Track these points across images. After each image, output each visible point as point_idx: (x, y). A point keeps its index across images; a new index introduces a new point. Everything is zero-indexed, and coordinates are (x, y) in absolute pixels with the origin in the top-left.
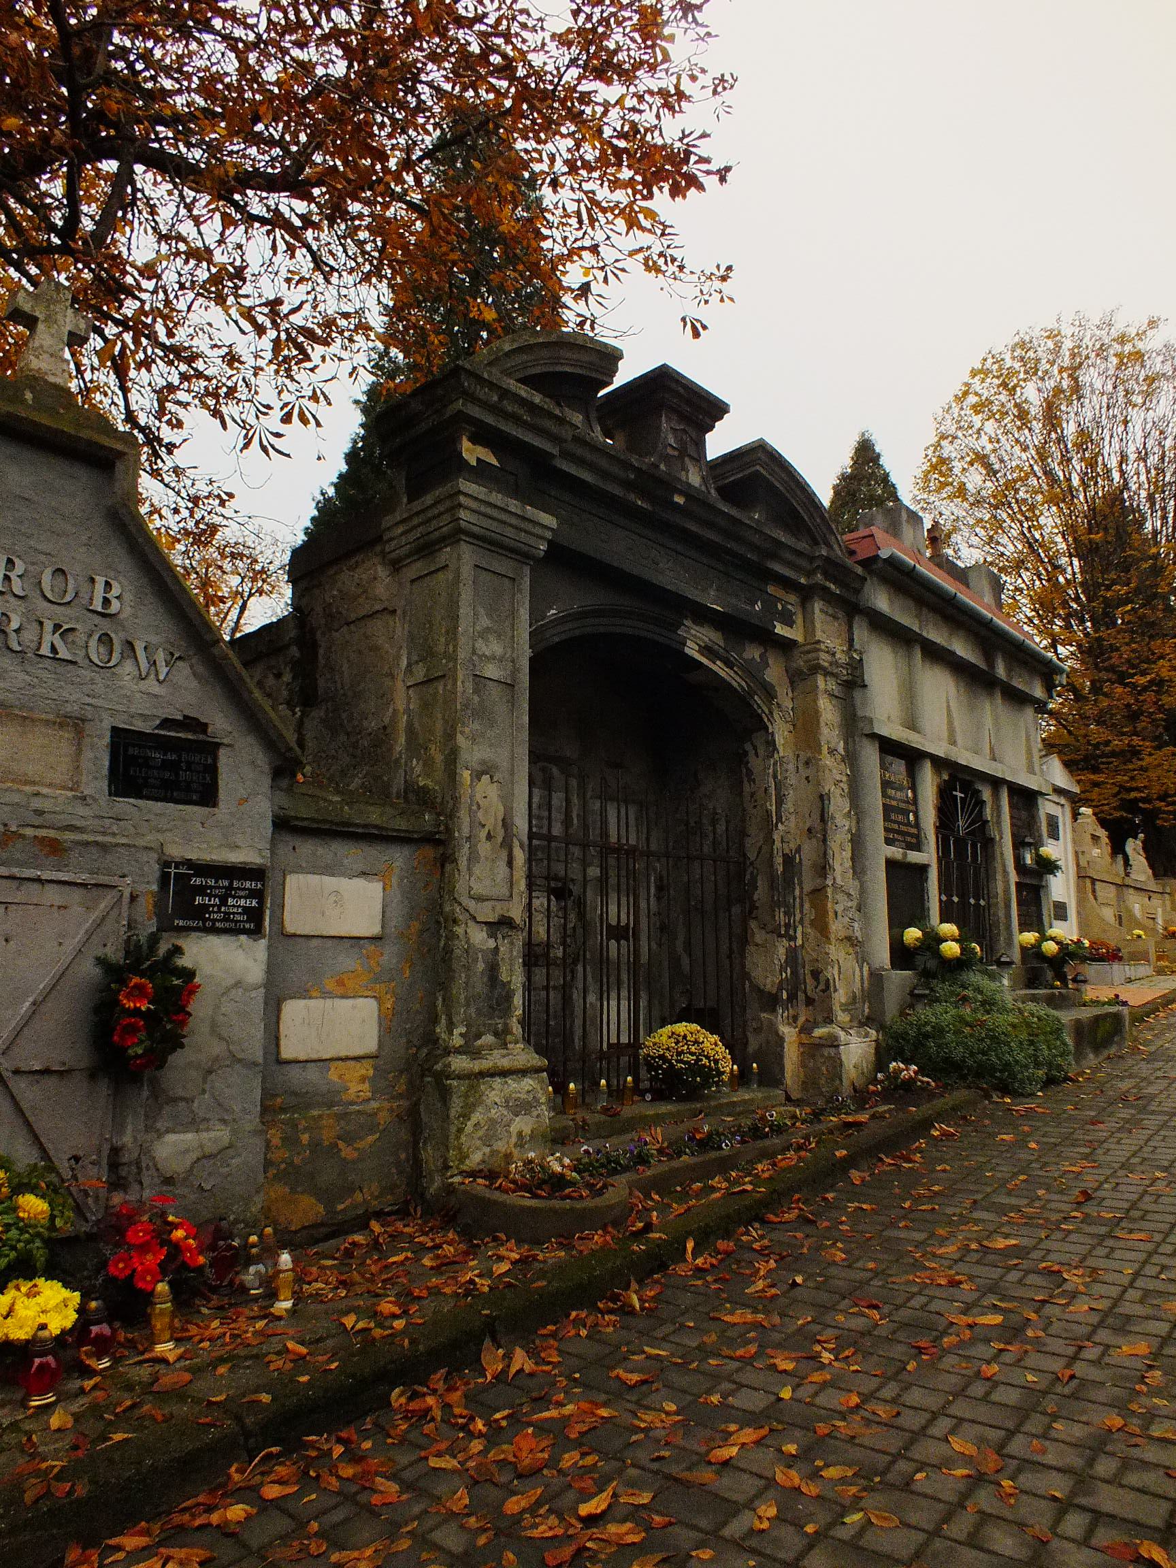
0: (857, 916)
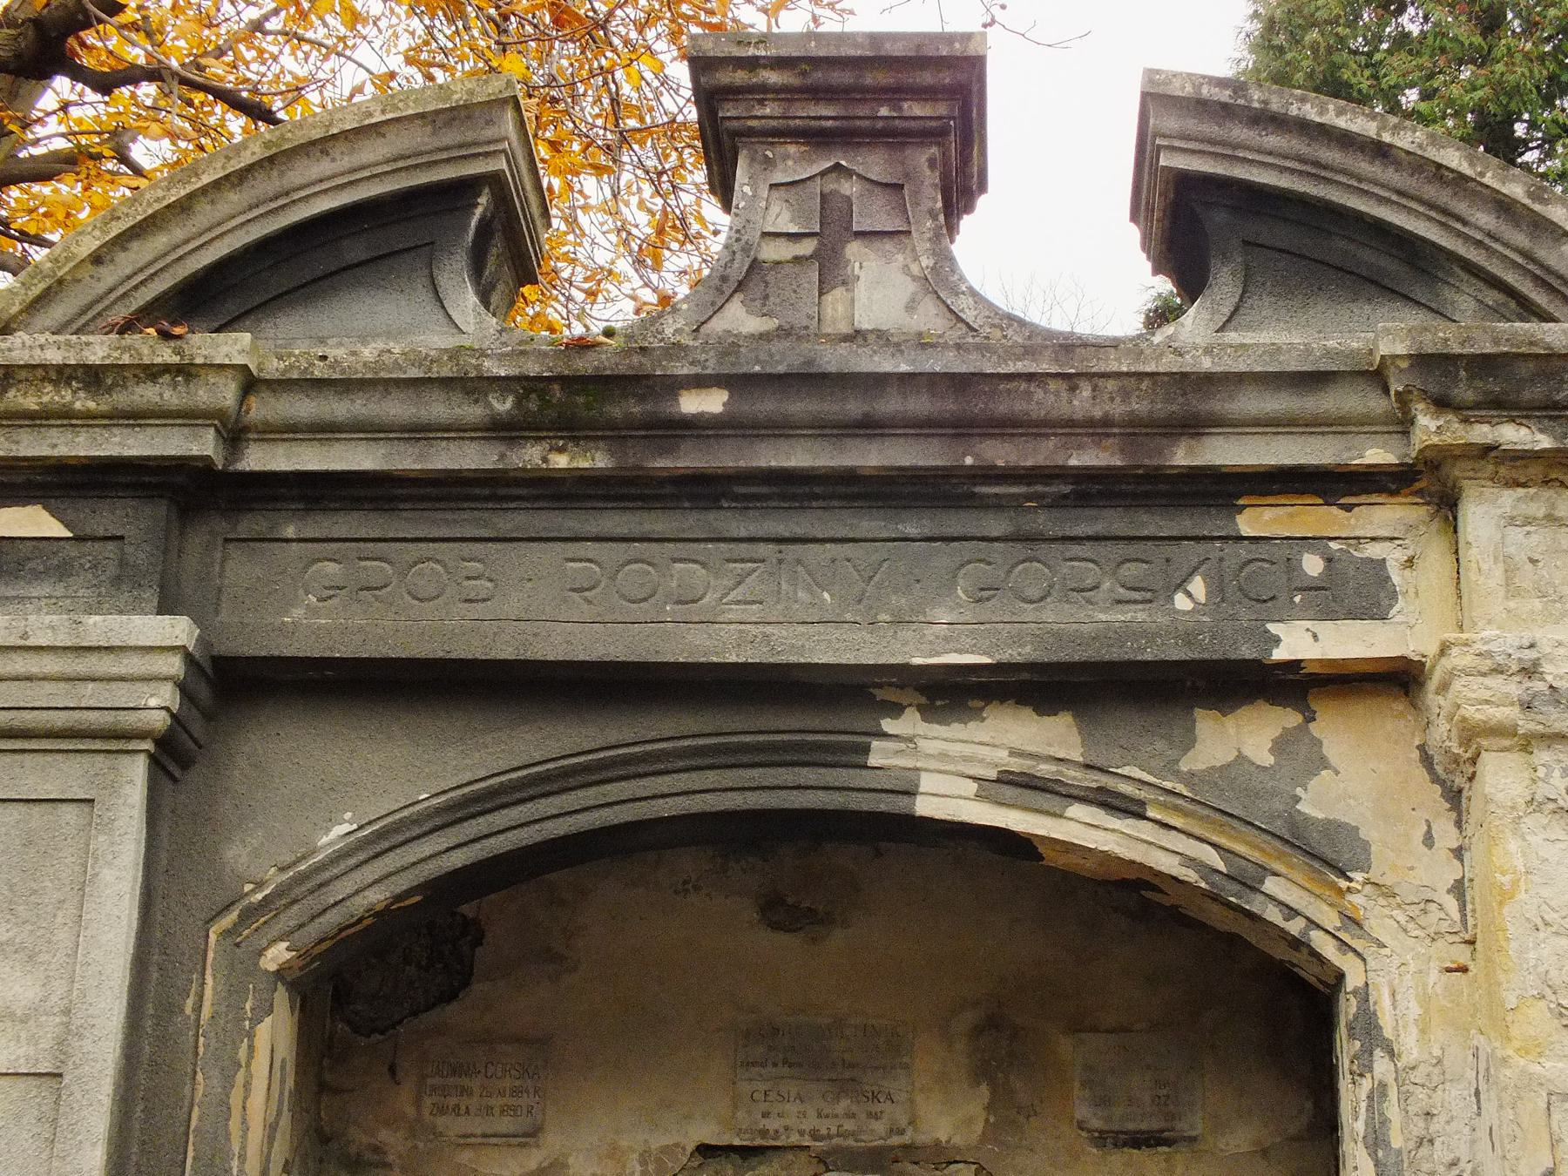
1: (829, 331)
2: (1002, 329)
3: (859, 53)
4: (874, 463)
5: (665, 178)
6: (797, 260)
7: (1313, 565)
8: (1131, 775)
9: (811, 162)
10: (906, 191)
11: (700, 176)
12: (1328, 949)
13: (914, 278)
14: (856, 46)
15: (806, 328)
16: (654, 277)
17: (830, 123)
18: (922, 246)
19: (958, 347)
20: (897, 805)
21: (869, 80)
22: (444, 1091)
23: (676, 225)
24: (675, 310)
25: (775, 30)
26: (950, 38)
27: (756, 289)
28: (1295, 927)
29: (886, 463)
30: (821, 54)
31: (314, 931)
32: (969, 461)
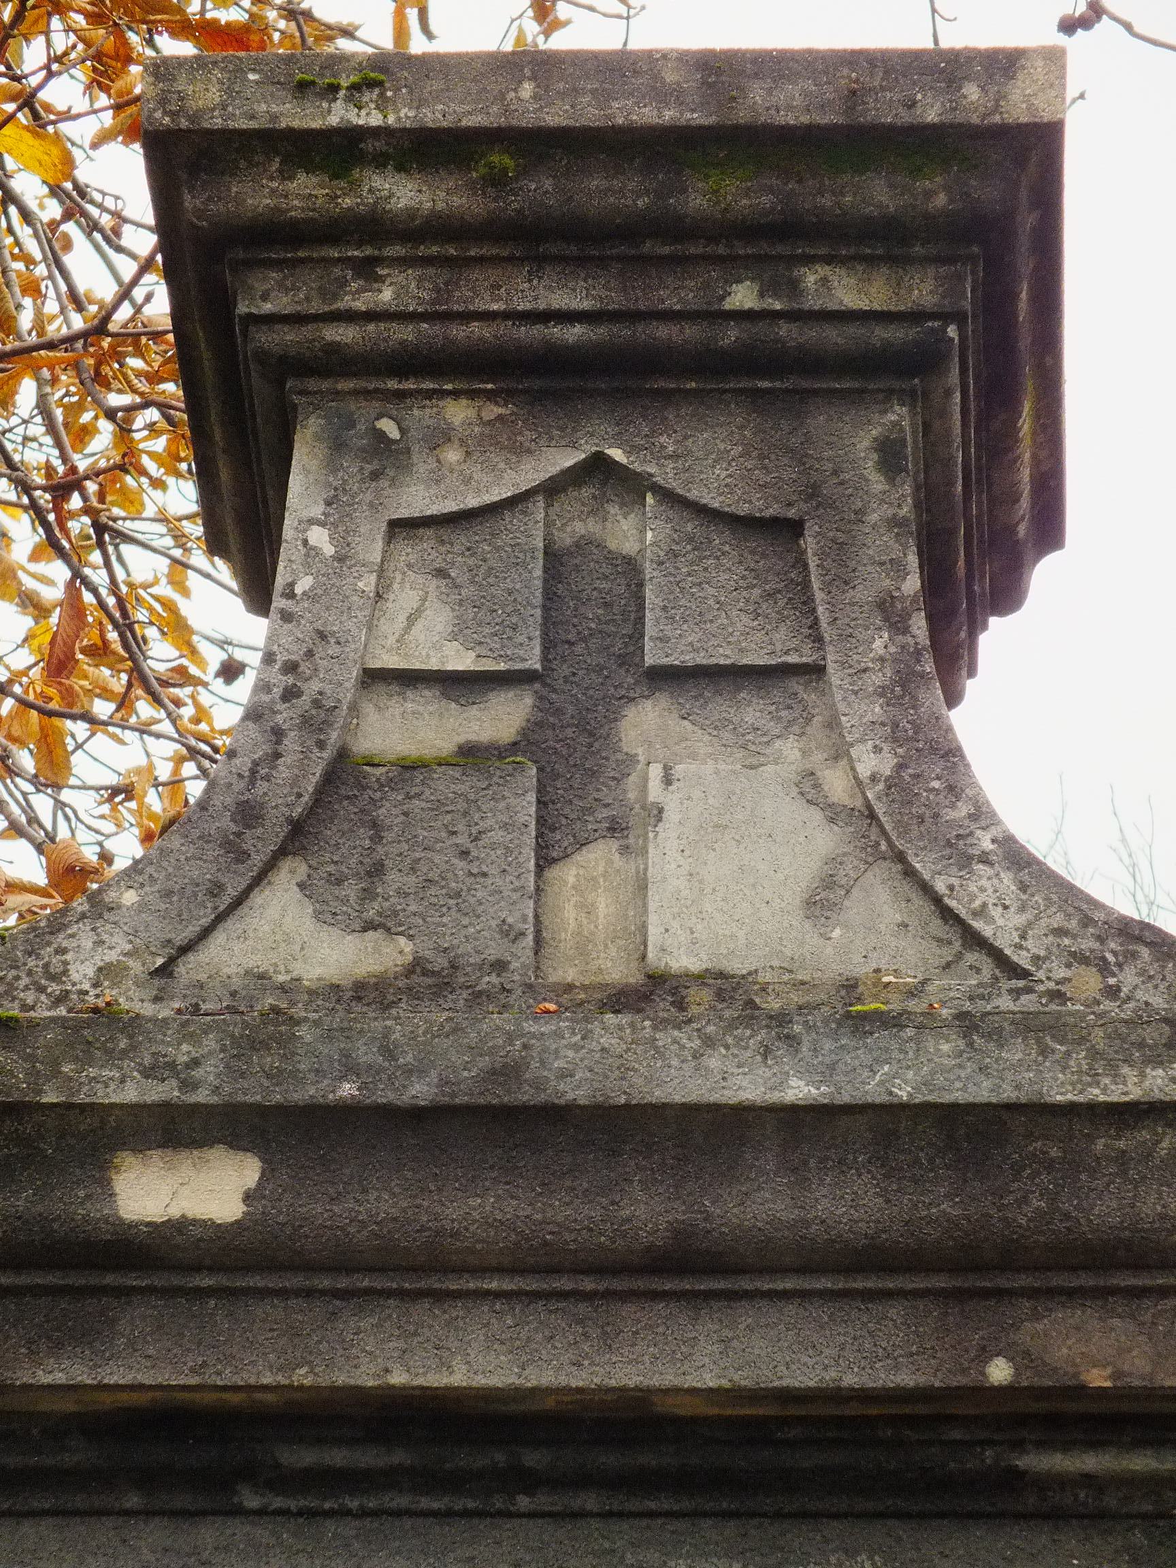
1: (571, 975)
2: (1104, 969)
3: (669, 115)
4: (710, 1380)
5: (76, 502)
6: (471, 755)
9: (520, 451)
10: (809, 543)
11: (183, 496)
13: (833, 813)
14: (662, 94)
15: (500, 966)
16: (43, 804)
17: (575, 333)
18: (861, 711)
19: (967, 1023)
21: (697, 200)
23: (95, 650)
24: (99, 908)
25: (418, 45)
26: (946, 68)
27: (345, 845)
29: (744, 1379)
30: (555, 117)
32: (999, 1372)
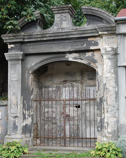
0: (117, 111)
7: (93, 42)
8: (82, 57)
12: (95, 68)
20: (67, 60)
22: (46, 78)
28: (93, 67)
31: (33, 70)
